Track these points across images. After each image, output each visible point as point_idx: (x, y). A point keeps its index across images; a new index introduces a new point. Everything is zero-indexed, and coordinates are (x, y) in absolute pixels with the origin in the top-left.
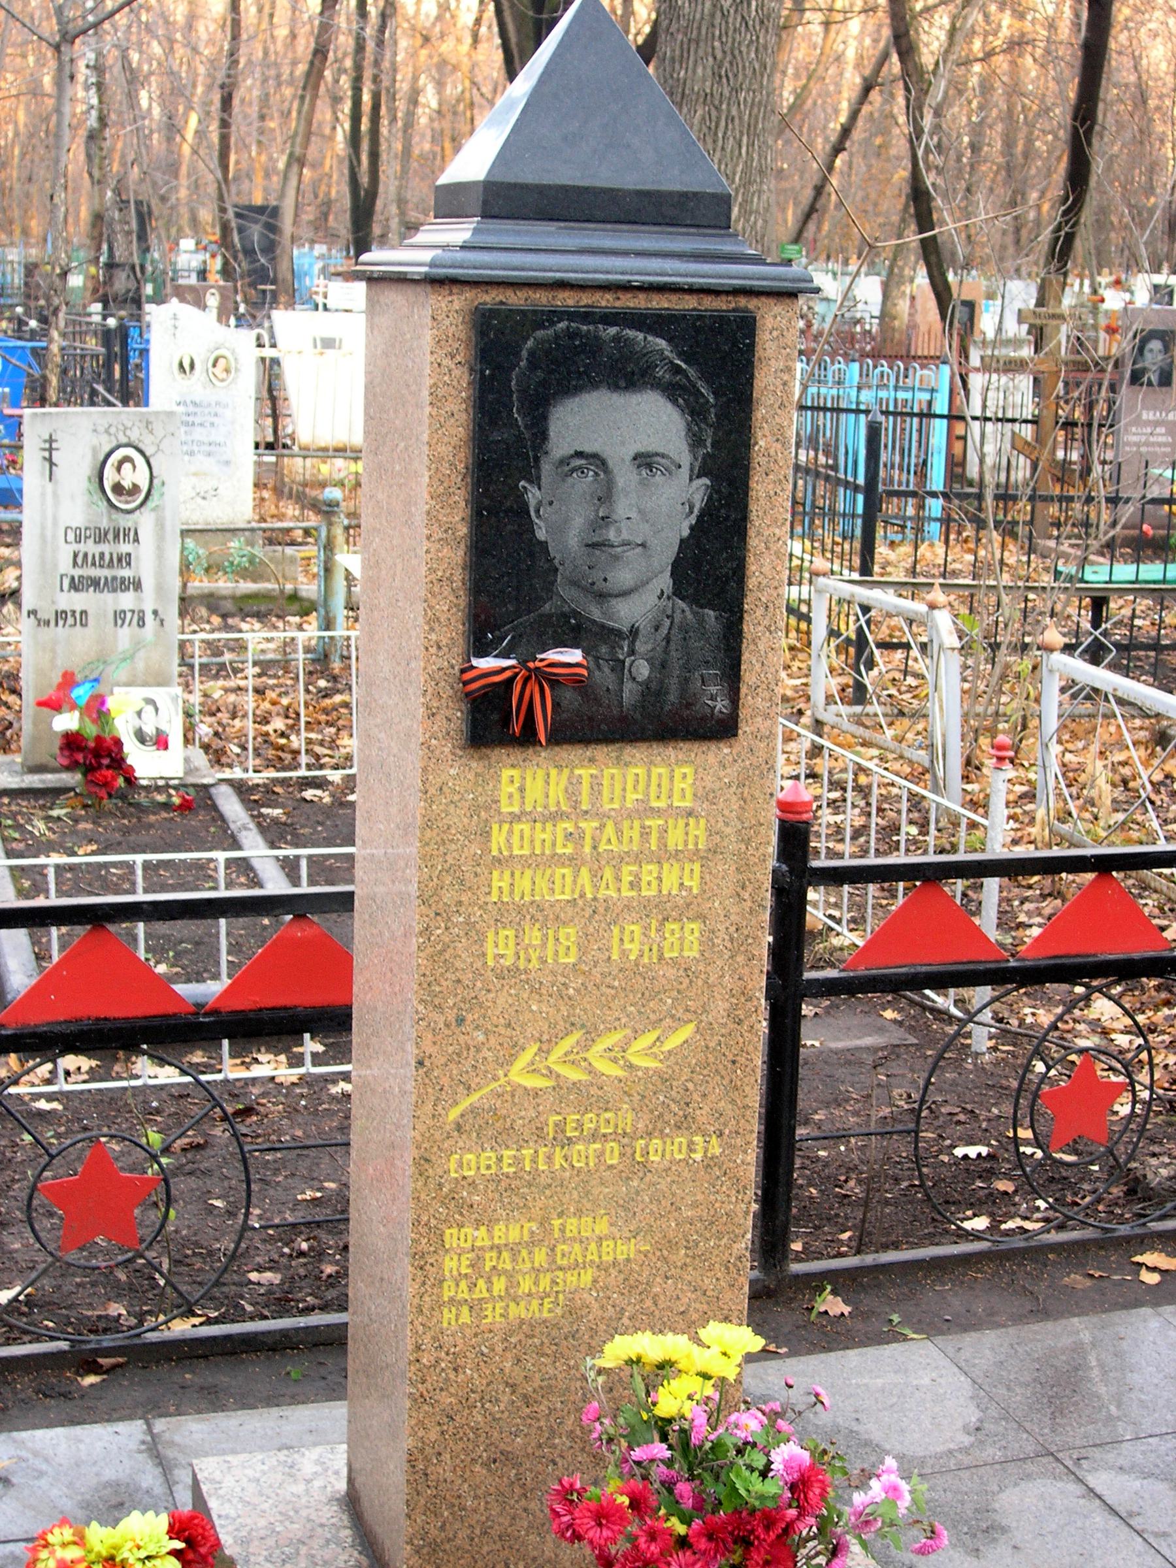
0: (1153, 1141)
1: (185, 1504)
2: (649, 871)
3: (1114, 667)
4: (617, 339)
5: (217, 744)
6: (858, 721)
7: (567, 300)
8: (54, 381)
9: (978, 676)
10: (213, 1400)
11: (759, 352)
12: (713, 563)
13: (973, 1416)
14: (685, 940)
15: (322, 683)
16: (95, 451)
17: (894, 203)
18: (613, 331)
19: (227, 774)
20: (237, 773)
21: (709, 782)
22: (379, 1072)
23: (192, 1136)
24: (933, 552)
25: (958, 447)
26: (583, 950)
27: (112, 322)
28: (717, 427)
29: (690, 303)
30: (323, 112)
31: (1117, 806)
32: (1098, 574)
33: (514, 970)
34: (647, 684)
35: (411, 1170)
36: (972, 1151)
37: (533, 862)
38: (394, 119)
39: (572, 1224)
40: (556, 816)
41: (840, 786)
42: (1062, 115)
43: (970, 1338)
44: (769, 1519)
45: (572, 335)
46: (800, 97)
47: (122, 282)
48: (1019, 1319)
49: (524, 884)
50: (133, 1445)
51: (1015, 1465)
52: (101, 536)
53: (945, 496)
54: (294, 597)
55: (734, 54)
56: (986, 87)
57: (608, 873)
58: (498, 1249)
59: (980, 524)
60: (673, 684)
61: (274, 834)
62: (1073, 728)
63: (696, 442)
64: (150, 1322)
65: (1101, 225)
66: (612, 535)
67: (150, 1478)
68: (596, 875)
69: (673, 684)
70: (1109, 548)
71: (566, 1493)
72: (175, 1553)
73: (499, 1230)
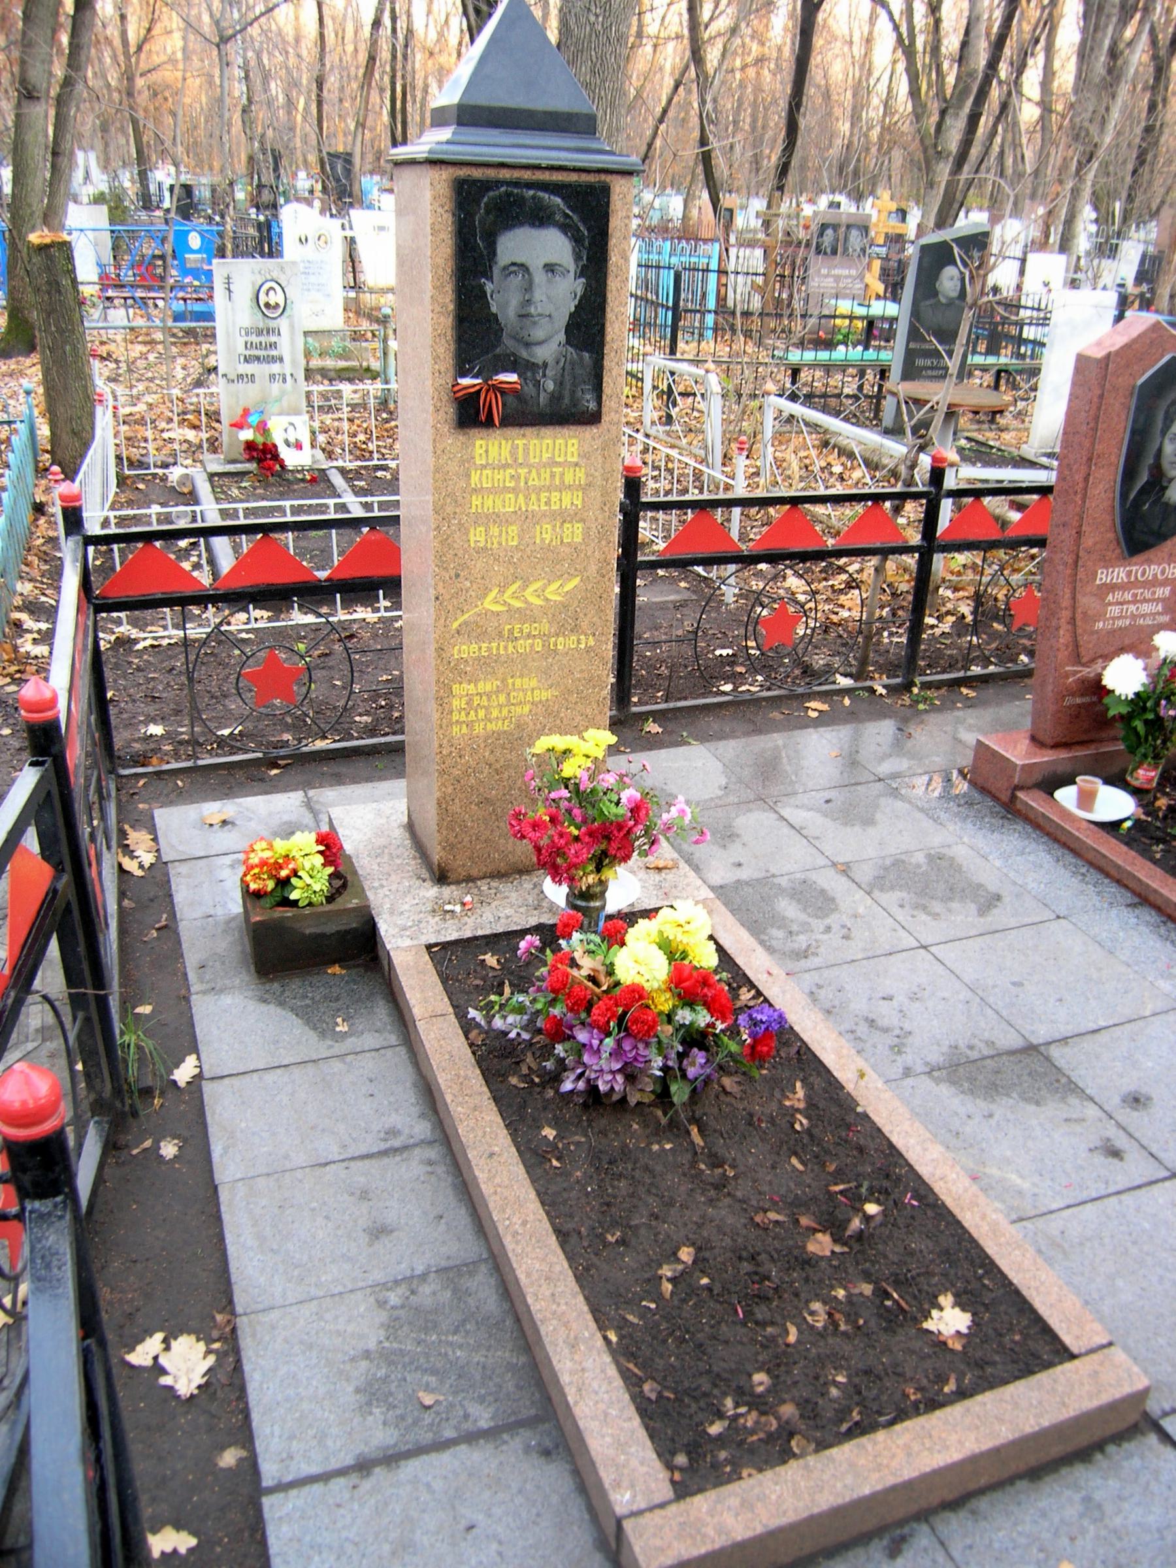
0: (816, 647)
1: (325, 828)
2: (555, 496)
3: (803, 404)
4: (534, 197)
5: (329, 448)
6: (668, 433)
7: (505, 174)
8: (229, 246)
9: (731, 411)
10: (338, 780)
11: (612, 207)
12: (587, 327)
13: (723, 781)
14: (574, 533)
15: (385, 415)
16: (253, 284)
17: (691, 152)
18: (531, 192)
19: (335, 464)
20: (340, 463)
21: (586, 448)
22: (417, 614)
23: (322, 649)
24: (708, 345)
25: (723, 290)
26: (521, 538)
27: (262, 218)
28: (589, 249)
29: (573, 177)
30: (375, 97)
31: (802, 479)
32: (795, 356)
33: (485, 549)
34: (552, 394)
35: (434, 654)
36: (724, 652)
37: (492, 491)
38: (414, 101)
39: (518, 682)
40: (505, 466)
41: (658, 468)
42: (783, 104)
43: (722, 744)
44: (620, 826)
45: (508, 195)
46: (638, 95)
47: (266, 196)
48: (747, 734)
49: (489, 503)
50: (298, 803)
51: (744, 805)
52: (260, 332)
53: (716, 312)
54: (368, 369)
55: (602, 58)
56: (742, 85)
57: (533, 497)
58: (480, 695)
59: (733, 331)
60: (567, 393)
61: (358, 492)
62: (780, 438)
63: (577, 257)
64: (304, 742)
65: (803, 167)
66: (532, 310)
67: (308, 818)
68: (527, 498)
69: (567, 393)
70: (802, 345)
71: (517, 815)
72: (320, 852)
73: (481, 685)
